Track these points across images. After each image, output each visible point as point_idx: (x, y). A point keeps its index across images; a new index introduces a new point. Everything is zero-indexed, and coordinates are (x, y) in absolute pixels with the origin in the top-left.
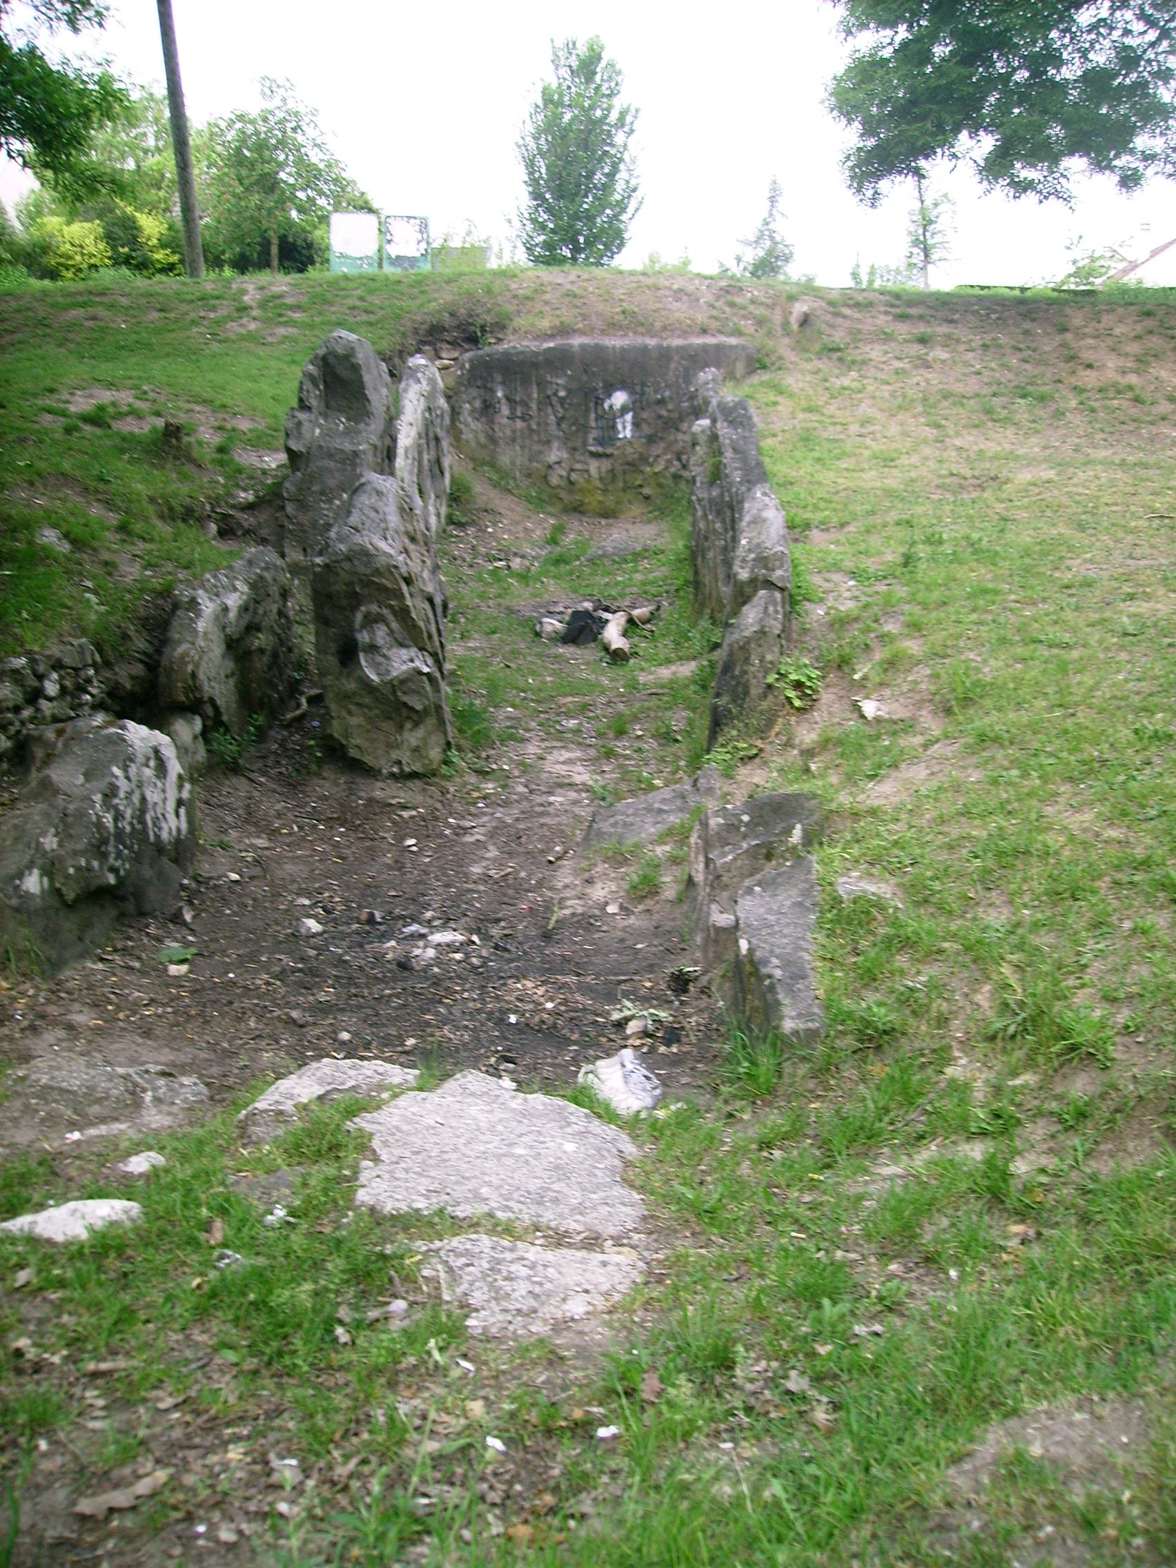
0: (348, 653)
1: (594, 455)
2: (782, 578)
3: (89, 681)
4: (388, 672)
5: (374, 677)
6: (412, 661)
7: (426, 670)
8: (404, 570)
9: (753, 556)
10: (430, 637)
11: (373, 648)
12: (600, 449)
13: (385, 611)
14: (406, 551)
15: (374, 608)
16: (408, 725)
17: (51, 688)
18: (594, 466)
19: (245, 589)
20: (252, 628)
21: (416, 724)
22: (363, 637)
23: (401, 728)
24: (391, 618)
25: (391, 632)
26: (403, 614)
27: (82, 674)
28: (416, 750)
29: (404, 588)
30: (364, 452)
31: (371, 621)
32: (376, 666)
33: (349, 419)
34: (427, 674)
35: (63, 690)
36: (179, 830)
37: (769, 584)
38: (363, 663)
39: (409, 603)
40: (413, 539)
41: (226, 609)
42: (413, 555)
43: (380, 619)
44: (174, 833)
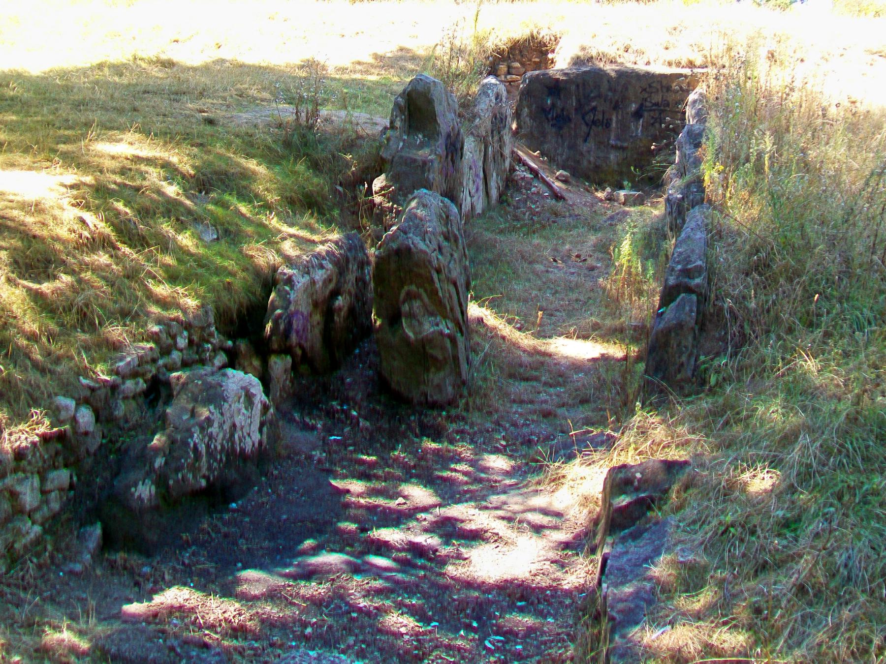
0: (394, 318)
1: (615, 148)
2: (698, 285)
3: (211, 335)
4: (420, 333)
5: (411, 334)
6: (437, 325)
7: (447, 331)
8: (435, 263)
9: (679, 267)
10: (452, 309)
11: (411, 316)
12: (619, 144)
13: (421, 291)
14: (440, 249)
15: (413, 288)
16: (433, 369)
17: (182, 342)
18: (613, 156)
19: (330, 266)
20: (335, 294)
21: (439, 369)
22: (405, 308)
23: (428, 370)
24: (424, 296)
25: (424, 306)
26: (433, 293)
27: (207, 331)
28: (438, 386)
29: (435, 276)
30: (432, 161)
31: (410, 296)
32: (411, 326)
33: (424, 136)
34: (449, 336)
35: (191, 342)
36: (260, 443)
37: (689, 290)
38: (404, 325)
39: (438, 285)
40: (447, 238)
41: (313, 282)
42: (444, 251)
43: (417, 296)
44: (256, 445)
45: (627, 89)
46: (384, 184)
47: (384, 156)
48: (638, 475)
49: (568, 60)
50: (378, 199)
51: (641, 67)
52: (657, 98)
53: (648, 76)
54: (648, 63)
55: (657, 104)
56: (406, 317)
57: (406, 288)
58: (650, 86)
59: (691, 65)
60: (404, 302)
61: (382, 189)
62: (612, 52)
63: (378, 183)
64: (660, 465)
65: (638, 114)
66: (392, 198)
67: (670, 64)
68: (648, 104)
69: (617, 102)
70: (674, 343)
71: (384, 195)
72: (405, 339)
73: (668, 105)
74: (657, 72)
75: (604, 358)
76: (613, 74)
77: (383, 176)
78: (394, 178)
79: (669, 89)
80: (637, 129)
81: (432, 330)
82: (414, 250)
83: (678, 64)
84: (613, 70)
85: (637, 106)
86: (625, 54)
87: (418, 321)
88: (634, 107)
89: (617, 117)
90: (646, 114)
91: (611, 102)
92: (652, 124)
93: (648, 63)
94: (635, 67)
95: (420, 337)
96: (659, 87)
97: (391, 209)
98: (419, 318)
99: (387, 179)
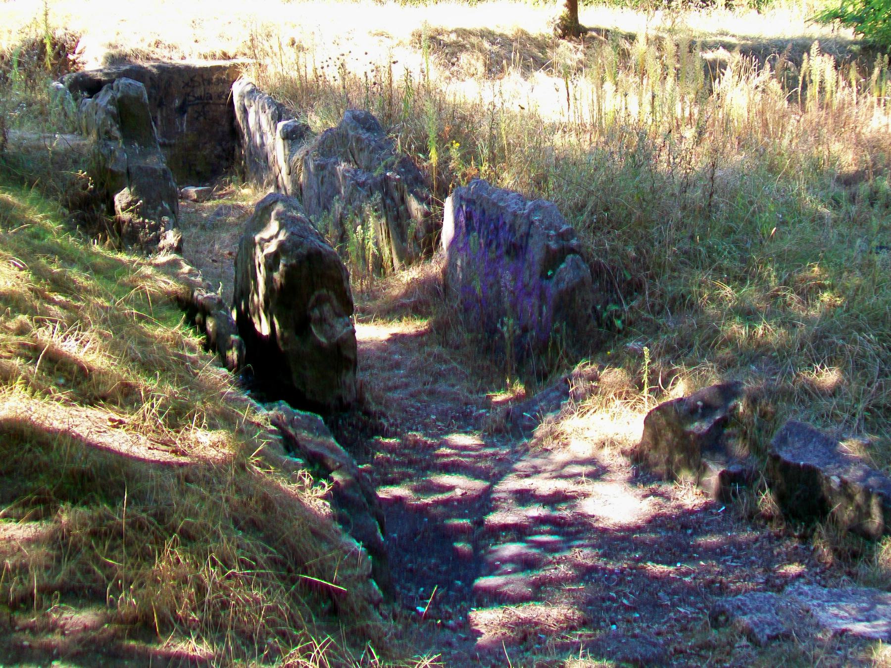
5: (323, 340)
13: (331, 293)
22: (316, 313)
31: (320, 301)
33: (140, 145)
43: (328, 300)
45: (170, 85)
46: (130, 198)
47: (115, 169)
48: (699, 403)
49: (102, 60)
50: (126, 216)
51: (177, 61)
52: (200, 92)
53: (188, 69)
54: (183, 58)
55: (200, 98)
56: (315, 324)
57: (317, 293)
58: (192, 80)
59: (225, 56)
60: (313, 307)
61: (129, 204)
62: (145, 48)
63: (122, 198)
64: (716, 390)
65: (182, 110)
66: (142, 212)
67: (206, 58)
68: (191, 98)
69: (161, 99)
70: (578, 299)
71: (132, 211)
72: (319, 346)
73: (211, 98)
74: (198, 66)
75: (396, 339)
76: (155, 70)
77: (126, 191)
78: (140, 192)
79: (210, 82)
80: (182, 125)
81: (345, 331)
82: (324, 252)
83: (214, 56)
84: (154, 66)
85: (181, 101)
86: (157, 50)
87: (329, 324)
88: (177, 103)
89: (162, 115)
90: (190, 109)
91: (155, 99)
92: (197, 118)
93: (183, 58)
94: (173, 62)
95: (334, 340)
96: (201, 81)
97: (143, 225)
98: (330, 320)
99: (132, 194)
